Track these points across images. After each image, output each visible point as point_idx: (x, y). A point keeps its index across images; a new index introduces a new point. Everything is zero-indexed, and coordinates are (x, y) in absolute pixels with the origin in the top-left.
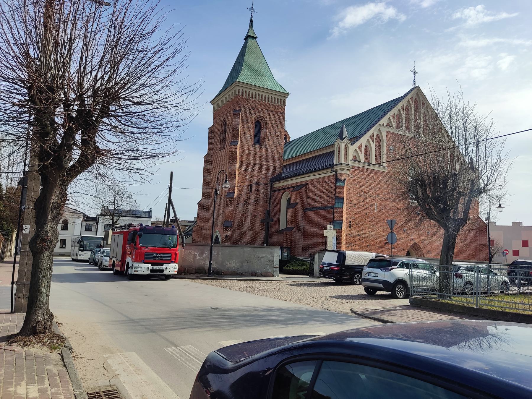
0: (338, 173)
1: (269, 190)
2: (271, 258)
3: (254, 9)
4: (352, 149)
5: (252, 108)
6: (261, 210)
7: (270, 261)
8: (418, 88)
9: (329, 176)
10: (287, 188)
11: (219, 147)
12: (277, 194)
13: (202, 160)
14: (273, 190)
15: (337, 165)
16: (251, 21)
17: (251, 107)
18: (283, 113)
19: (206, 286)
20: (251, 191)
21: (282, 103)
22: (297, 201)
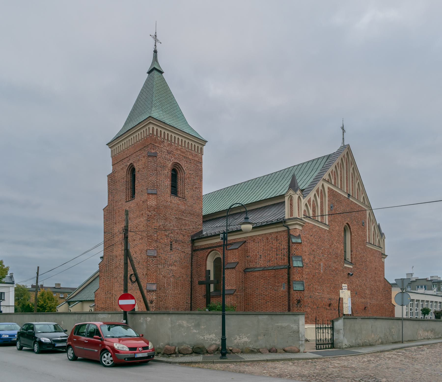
0: (291, 227)
1: (190, 249)
2: (295, 327)
3: (158, 38)
4: (304, 201)
5: (169, 152)
6: (183, 271)
7: (294, 332)
8: (348, 147)
9: (277, 232)
10: (216, 247)
11: (124, 197)
12: (201, 254)
13: (101, 214)
14: (194, 250)
15: (289, 219)
16: (155, 52)
17: (167, 151)
18: (201, 163)
19: (199, 370)
20: (171, 249)
21: (200, 152)
22: (238, 260)
